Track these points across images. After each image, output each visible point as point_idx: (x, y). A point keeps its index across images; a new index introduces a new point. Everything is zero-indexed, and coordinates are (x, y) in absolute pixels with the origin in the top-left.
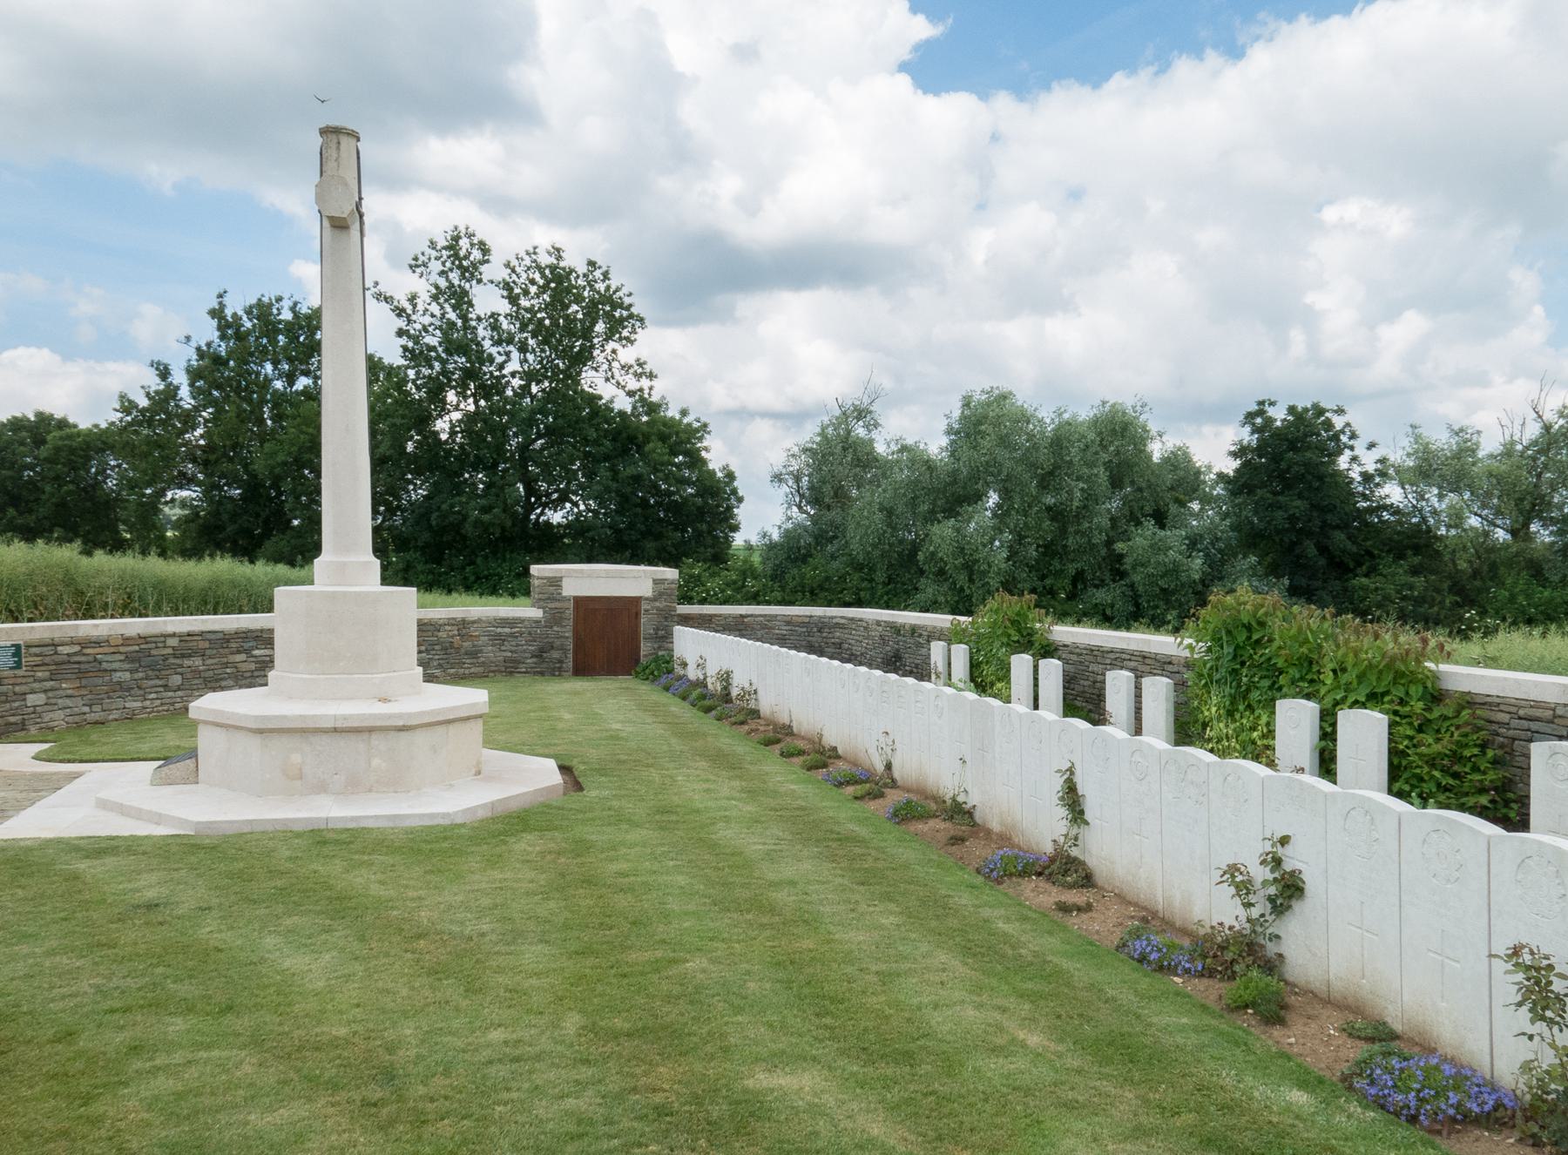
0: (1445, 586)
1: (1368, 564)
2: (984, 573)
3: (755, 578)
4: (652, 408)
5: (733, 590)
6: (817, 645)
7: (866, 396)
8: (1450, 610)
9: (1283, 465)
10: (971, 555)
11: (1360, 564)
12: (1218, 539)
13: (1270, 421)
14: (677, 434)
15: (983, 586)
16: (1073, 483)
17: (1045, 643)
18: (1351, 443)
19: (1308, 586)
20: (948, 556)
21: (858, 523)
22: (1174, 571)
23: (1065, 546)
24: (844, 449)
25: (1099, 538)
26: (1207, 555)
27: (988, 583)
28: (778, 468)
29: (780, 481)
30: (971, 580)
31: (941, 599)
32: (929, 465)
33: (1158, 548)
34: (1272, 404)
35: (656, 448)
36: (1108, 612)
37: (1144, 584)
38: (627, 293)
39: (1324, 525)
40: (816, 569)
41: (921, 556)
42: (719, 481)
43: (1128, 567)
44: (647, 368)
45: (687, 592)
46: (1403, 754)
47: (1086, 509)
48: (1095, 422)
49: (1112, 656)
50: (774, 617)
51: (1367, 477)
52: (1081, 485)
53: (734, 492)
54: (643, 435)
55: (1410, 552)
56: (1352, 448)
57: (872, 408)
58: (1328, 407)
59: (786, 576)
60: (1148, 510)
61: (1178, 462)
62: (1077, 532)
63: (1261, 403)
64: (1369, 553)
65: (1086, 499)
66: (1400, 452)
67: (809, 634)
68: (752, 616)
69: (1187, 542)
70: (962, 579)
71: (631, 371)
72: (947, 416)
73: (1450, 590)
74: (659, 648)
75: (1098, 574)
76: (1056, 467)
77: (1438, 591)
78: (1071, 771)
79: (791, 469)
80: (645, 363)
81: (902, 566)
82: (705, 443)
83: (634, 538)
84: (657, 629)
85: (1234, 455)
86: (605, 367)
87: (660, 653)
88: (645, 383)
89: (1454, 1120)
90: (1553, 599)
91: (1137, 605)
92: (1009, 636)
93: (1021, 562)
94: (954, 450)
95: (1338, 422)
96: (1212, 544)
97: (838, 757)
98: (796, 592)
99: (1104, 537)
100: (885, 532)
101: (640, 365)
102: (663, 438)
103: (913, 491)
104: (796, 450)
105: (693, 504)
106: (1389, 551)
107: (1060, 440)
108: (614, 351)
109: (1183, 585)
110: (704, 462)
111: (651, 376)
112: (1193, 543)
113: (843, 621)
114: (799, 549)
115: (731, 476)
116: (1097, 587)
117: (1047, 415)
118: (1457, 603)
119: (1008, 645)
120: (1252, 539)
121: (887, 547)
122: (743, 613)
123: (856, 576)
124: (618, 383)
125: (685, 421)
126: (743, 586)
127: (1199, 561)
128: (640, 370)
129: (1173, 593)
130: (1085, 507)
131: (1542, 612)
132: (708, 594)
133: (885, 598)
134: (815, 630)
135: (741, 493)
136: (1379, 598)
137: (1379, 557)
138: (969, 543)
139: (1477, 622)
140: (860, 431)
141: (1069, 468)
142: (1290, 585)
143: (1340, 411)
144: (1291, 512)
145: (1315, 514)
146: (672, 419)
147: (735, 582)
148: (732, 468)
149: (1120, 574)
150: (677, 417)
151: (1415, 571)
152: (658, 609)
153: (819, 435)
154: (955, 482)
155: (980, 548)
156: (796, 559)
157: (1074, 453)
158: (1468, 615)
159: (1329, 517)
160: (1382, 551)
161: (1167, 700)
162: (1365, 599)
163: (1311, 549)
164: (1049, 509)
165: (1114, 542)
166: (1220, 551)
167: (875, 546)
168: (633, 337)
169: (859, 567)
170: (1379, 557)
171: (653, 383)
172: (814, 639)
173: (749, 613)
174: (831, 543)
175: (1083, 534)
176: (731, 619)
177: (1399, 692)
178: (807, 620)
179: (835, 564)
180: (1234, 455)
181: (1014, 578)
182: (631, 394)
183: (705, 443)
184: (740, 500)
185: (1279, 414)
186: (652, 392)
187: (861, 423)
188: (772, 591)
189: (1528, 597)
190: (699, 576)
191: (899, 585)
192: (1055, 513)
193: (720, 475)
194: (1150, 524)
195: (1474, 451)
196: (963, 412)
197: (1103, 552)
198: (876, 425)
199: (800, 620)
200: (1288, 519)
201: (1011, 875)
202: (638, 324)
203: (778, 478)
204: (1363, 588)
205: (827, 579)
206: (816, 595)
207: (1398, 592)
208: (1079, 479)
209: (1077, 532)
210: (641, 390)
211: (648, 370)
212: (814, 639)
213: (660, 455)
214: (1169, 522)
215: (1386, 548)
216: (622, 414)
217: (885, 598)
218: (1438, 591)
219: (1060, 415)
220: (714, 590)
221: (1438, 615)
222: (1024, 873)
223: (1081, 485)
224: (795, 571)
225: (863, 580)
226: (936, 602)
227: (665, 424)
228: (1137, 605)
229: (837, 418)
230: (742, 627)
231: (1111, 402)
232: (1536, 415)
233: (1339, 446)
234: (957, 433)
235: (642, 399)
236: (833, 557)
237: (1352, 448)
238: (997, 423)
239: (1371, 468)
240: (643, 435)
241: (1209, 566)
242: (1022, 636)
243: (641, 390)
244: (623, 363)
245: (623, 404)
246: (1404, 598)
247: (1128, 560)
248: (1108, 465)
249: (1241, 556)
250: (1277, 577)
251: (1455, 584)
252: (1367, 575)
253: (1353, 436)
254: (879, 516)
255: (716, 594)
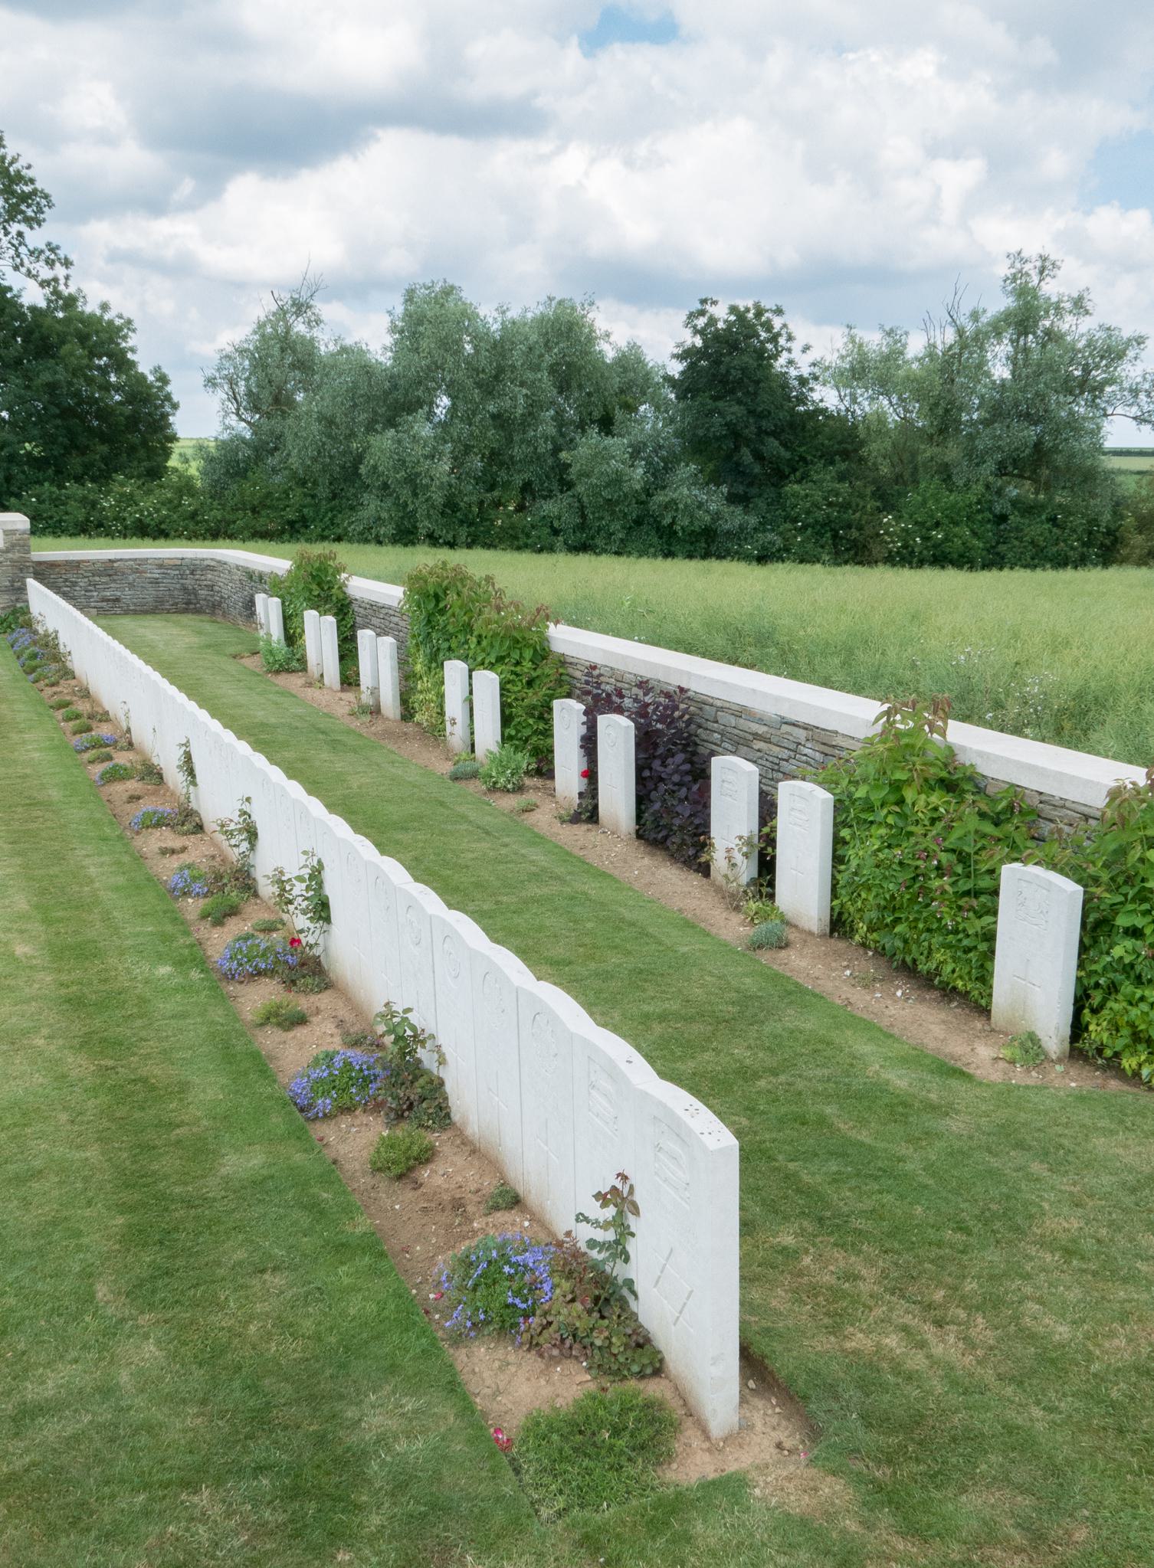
0: (868, 491)
1: (801, 470)
2: (427, 487)
3: (193, 496)
4: (70, 302)
5: (169, 510)
6: (190, 587)
7: (305, 288)
8: (872, 514)
9: (723, 369)
10: (413, 468)
11: (794, 470)
12: (661, 447)
13: (712, 321)
14: (97, 333)
15: (427, 500)
16: (517, 389)
17: (341, 596)
18: (789, 345)
19: (746, 493)
20: (389, 470)
21: (296, 434)
22: (617, 480)
23: (512, 457)
24: (283, 350)
25: (545, 447)
26: (649, 464)
27: (430, 497)
28: (210, 372)
29: (215, 385)
30: (415, 495)
31: (384, 515)
32: (367, 370)
33: (603, 456)
34: (714, 303)
35: (74, 350)
36: (556, 524)
37: (588, 496)
38: (25, 165)
39: (761, 432)
40: (255, 485)
41: (363, 470)
42: (151, 386)
43: (574, 477)
44: (61, 253)
45: (119, 512)
46: (510, 706)
47: (531, 415)
48: (541, 321)
49: (384, 611)
50: (144, 561)
51: (803, 381)
52: (525, 391)
53: (168, 397)
54: (58, 335)
55: (837, 458)
56: (789, 350)
57: (312, 302)
58: (767, 307)
59: (226, 493)
60: (597, 415)
61: (630, 363)
62: (522, 441)
63: (704, 302)
64: (803, 459)
65: (531, 405)
66: (836, 355)
67: (182, 576)
68: (121, 560)
69: (630, 450)
70: (405, 493)
71: (43, 257)
72: (390, 313)
73: (873, 494)
74: (17, 600)
75: (546, 484)
76: (500, 370)
77: (862, 496)
78: (187, 744)
79: (226, 372)
80: (58, 247)
81: (345, 481)
82: (131, 343)
83: (56, 453)
84: (12, 581)
85: (680, 357)
86: (12, 252)
87: (18, 605)
88: (60, 271)
89: (252, 975)
90: (957, 503)
91: (583, 516)
92: (311, 591)
93: (467, 473)
94: (399, 350)
95: (777, 323)
96: (655, 451)
97: (108, 720)
98: (237, 510)
99: (550, 447)
100: (324, 444)
101: (52, 250)
102: (83, 338)
103: (353, 399)
104: (229, 349)
105: (121, 414)
106: (821, 457)
107: (500, 347)
108: (20, 234)
109: (626, 495)
110: (132, 364)
111: (67, 263)
112: (636, 452)
113: (213, 563)
114: (238, 462)
115: (164, 380)
116: (545, 498)
117: (490, 316)
118: (878, 508)
119: (310, 599)
120: (698, 446)
121: (328, 460)
122: (112, 557)
123: (299, 491)
124: (29, 271)
125: (106, 317)
126: (180, 505)
127: (640, 471)
128: (52, 257)
129: (618, 502)
130: (530, 414)
131: (947, 517)
132: (142, 515)
133: (330, 515)
134: (188, 572)
135: (175, 398)
136: (808, 505)
137: (812, 462)
138: (409, 455)
139: (893, 526)
140: (299, 327)
141: (512, 372)
142: (729, 492)
143: (779, 312)
144: (728, 419)
145: (751, 420)
146: (92, 315)
147: (170, 501)
148: (165, 370)
149: (567, 485)
150: (98, 312)
151: (842, 477)
152: (12, 560)
153: (255, 333)
154: (395, 387)
155: (422, 460)
156: (237, 474)
157: (517, 357)
158: (885, 520)
159: (764, 423)
160: (814, 456)
161: (391, 658)
162: (796, 506)
163: (746, 456)
164: (494, 417)
165: (561, 450)
166: (662, 459)
167: (314, 460)
168: (42, 216)
169: (303, 483)
170: (812, 462)
171: (69, 272)
172: (188, 582)
173: (119, 557)
174: (272, 455)
175: (529, 443)
176: (99, 565)
177: (516, 655)
178: (179, 562)
179: (277, 479)
180: (680, 357)
181: (460, 492)
182: (44, 284)
183: (131, 343)
184: (175, 406)
185: (721, 312)
186: (70, 283)
187: (300, 319)
188: (211, 510)
189: (937, 501)
190: (131, 494)
191: (344, 500)
192: (500, 420)
193: (151, 378)
194: (594, 431)
195: (902, 353)
196: (406, 309)
197: (550, 461)
198: (318, 322)
199: (172, 562)
200: (726, 424)
201: (148, 827)
202: (44, 202)
203: (211, 383)
204: (795, 495)
205: (269, 494)
206: (258, 512)
207: (826, 499)
208: (522, 384)
209: (522, 441)
210: (56, 280)
211: (62, 256)
212: (188, 582)
213: (78, 358)
214: (615, 429)
215: (819, 453)
216: (33, 309)
217: (330, 515)
218: (862, 496)
219: (503, 313)
220: (148, 510)
221: (860, 520)
222: (158, 825)
223: (525, 391)
224: (235, 487)
225: (305, 495)
226: (379, 518)
227: (82, 321)
228: (583, 516)
229: (274, 314)
230: (111, 572)
231: (558, 298)
232: (950, 319)
233: (777, 350)
234: (401, 332)
235: (56, 292)
236: (275, 471)
237: (789, 350)
238: (439, 321)
239: (805, 371)
240: (58, 335)
241: (653, 475)
242: (323, 589)
243: (56, 280)
244: (32, 249)
245: (32, 296)
246: (830, 505)
247: (574, 470)
248: (553, 370)
249: (683, 464)
250: (718, 485)
251: (878, 489)
252: (799, 482)
253: (790, 338)
254: (315, 427)
255: (150, 514)
